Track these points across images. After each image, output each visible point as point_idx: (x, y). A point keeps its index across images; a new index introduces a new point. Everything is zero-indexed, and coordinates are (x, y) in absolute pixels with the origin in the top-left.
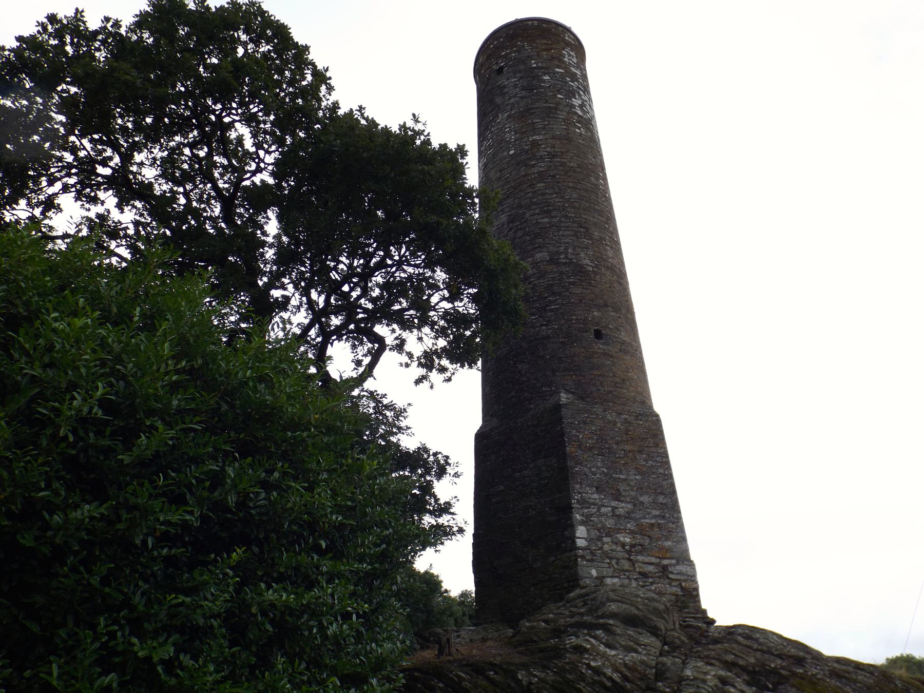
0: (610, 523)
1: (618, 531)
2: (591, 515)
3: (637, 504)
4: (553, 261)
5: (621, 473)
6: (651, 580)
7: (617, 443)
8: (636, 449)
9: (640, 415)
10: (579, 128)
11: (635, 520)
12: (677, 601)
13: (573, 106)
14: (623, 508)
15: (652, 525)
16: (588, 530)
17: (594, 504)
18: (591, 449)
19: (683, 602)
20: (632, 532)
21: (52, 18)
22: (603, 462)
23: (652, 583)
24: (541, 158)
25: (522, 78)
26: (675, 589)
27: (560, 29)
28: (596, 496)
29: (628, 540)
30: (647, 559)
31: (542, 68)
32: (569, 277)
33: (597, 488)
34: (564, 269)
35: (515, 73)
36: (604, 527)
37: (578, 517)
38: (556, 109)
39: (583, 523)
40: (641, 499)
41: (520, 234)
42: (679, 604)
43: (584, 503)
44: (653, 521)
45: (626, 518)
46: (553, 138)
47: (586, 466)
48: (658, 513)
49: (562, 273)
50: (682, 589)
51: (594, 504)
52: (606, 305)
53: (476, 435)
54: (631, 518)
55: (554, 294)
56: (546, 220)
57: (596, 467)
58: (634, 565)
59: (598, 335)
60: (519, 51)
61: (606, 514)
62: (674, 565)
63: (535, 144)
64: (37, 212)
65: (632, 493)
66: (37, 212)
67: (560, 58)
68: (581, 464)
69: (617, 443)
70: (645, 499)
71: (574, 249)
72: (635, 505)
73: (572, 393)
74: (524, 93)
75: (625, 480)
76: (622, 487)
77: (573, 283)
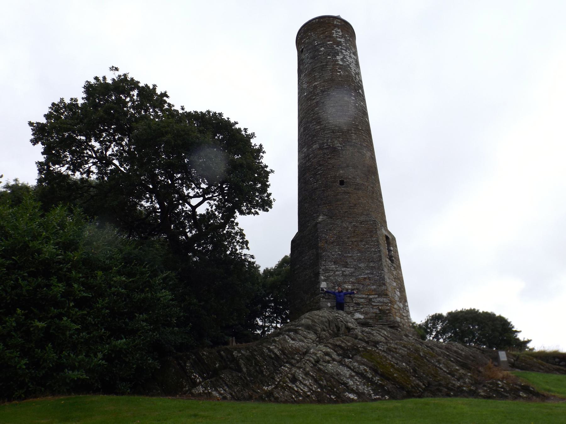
0: (340, 279)
1: (345, 283)
2: (330, 276)
3: (357, 268)
4: (321, 148)
5: (349, 253)
6: (361, 306)
7: (348, 238)
8: (359, 240)
9: (363, 221)
10: (340, 72)
11: (355, 276)
12: (376, 316)
13: (337, 60)
14: (348, 271)
15: (365, 278)
16: (327, 284)
17: (332, 270)
18: (332, 243)
19: (380, 316)
20: (353, 283)
21: (53, 104)
22: (339, 249)
23: (362, 308)
24: (318, 94)
25: (310, 52)
26: (375, 310)
27: (331, 19)
28: (333, 266)
29: (350, 287)
30: (360, 296)
31: (320, 44)
32: (328, 155)
33: (334, 262)
34: (325, 151)
35: (307, 50)
36: (337, 281)
37: (322, 277)
38: (326, 65)
39: (325, 280)
40: (360, 265)
41: (307, 136)
42: (377, 318)
43: (326, 270)
44: (366, 276)
45: (350, 276)
46: (324, 81)
47: (329, 252)
48: (369, 272)
49: (325, 154)
50: (380, 310)
51: (332, 270)
52: (348, 166)
53: (293, 242)
54: (353, 276)
55: (320, 165)
56: (318, 127)
57: (336, 251)
58: (352, 299)
59: (342, 183)
60: (309, 38)
61: (338, 275)
62: (376, 298)
63: (315, 87)
64: (85, 176)
65: (355, 263)
66: (85, 176)
67: (330, 37)
68: (326, 251)
69: (348, 238)
70: (362, 265)
71: (331, 140)
72: (356, 269)
73: (327, 215)
74: (311, 61)
75: (351, 256)
76: (349, 260)
77: (330, 158)
